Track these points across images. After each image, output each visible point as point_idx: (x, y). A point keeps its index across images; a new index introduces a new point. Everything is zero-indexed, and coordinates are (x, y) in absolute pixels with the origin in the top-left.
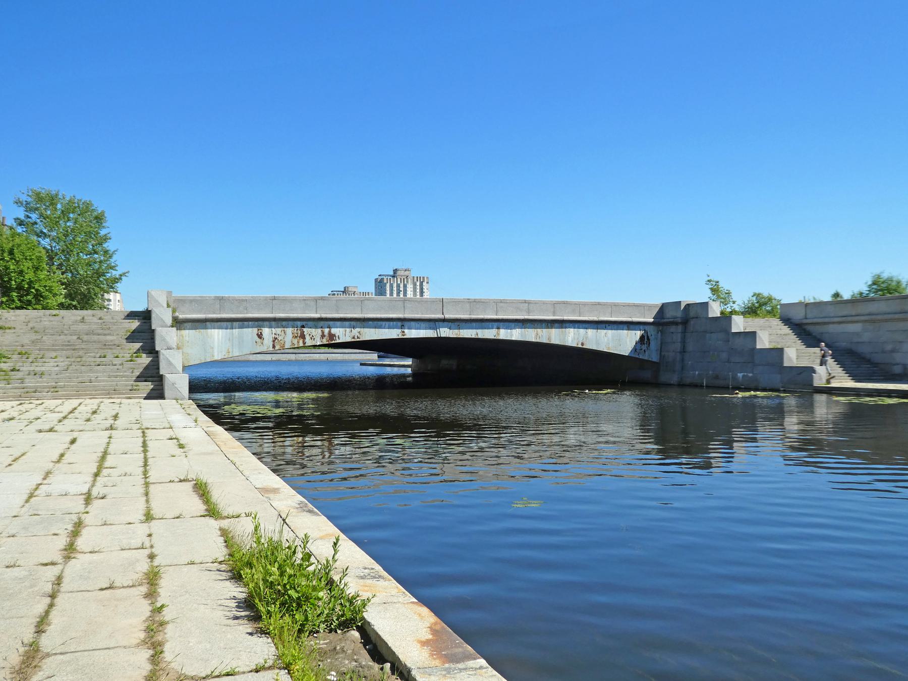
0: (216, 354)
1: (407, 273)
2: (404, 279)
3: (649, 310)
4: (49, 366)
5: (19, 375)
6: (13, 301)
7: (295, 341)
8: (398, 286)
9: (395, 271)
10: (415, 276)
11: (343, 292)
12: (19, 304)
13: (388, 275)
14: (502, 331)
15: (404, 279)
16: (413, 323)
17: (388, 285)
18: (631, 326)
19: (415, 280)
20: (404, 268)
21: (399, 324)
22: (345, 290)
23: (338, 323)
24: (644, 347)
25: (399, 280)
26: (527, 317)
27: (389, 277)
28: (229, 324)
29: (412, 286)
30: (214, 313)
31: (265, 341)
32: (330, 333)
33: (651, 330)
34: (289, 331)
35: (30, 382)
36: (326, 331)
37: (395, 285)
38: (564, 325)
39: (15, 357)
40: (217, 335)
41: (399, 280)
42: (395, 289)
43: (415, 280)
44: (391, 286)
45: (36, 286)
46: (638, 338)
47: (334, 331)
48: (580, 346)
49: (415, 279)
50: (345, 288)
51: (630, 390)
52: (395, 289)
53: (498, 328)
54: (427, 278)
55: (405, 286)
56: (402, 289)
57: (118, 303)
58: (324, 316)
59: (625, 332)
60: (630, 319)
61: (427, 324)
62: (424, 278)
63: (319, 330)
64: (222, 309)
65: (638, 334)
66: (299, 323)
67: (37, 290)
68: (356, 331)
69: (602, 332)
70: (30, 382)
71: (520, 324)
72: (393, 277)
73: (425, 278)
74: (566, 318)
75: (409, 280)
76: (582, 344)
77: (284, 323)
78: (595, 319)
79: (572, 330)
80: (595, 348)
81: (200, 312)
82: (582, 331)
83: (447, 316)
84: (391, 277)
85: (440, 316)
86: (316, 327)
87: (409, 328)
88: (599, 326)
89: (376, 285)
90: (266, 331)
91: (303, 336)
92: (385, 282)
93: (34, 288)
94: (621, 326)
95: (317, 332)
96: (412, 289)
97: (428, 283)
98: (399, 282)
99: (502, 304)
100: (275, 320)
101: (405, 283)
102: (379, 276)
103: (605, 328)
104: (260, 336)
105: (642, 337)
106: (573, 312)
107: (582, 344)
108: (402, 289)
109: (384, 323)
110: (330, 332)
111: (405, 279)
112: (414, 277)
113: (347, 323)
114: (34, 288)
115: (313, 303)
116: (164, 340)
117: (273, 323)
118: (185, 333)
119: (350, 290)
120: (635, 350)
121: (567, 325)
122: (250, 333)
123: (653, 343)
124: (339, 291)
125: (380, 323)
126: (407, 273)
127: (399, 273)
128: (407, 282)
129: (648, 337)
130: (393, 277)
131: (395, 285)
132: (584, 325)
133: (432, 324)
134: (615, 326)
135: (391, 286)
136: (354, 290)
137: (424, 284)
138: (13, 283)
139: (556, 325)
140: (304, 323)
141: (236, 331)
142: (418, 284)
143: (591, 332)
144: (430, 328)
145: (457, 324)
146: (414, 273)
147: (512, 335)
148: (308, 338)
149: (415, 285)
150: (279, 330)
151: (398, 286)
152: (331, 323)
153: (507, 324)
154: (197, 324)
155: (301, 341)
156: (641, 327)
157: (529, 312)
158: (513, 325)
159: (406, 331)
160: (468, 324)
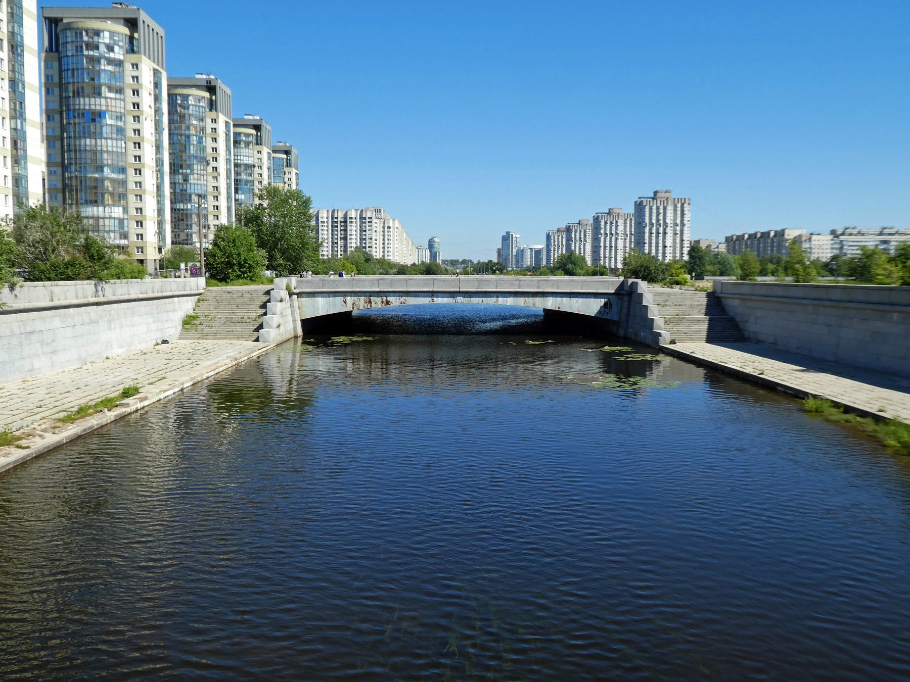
0: (320, 312)
1: (667, 195)
2: (664, 201)
3: (612, 284)
4: (217, 323)
5: (202, 327)
6: (236, 271)
7: (366, 305)
8: (658, 208)
9: (656, 193)
10: (626, 213)
11: (608, 213)
12: (239, 273)
13: (648, 198)
14: (500, 299)
15: (664, 201)
16: (439, 294)
17: (647, 208)
18: (597, 296)
19: (676, 202)
20: (665, 189)
21: (430, 294)
22: (609, 211)
23: (392, 294)
24: (607, 310)
25: (659, 202)
26: (517, 290)
27: (649, 199)
28: (328, 294)
29: (672, 208)
30: (319, 288)
31: (348, 305)
32: (386, 300)
33: (613, 298)
34: (362, 299)
35: (206, 331)
36: (384, 299)
37: (654, 208)
38: (545, 295)
39: (203, 318)
40: (320, 300)
41: (659, 202)
42: (654, 211)
43: (676, 202)
44: (651, 208)
45: (249, 262)
46: (602, 304)
47: (389, 299)
48: (557, 309)
49: (626, 215)
50: (579, 221)
51: (593, 345)
52: (654, 211)
53: (497, 297)
54: (689, 199)
55: (665, 208)
56: (661, 211)
57: (396, 230)
58: (382, 290)
59: (593, 299)
60: (595, 291)
61: (449, 295)
62: (685, 199)
63: (380, 298)
64: (323, 286)
65: (602, 302)
66: (368, 294)
67: (249, 264)
68: (402, 299)
69: (574, 300)
70: (206, 331)
71: (513, 295)
72: (653, 199)
73: (687, 200)
74: (546, 290)
75: (669, 202)
76: (559, 308)
77: (359, 294)
78: (568, 291)
79: (551, 298)
80: (568, 310)
81: (311, 288)
82: (559, 299)
83: (462, 290)
84: (651, 200)
85: (457, 290)
86: (378, 297)
87: (437, 297)
88: (572, 296)
89: (635, 207)
90: (349, 299)
91: (370, 302)
92: (644, 204)
93: (247, 263)
94: (589, 296)
95: (379, 300)
96: (672, 211)
97: (689, 204)
98: (659, 205)
99: (500, 282)
100: (353, 292)
101: (665, 205)
102: (639, 198)
103: (577, 297)
104: (345, 302)
105: (606, 304)
106: (553, 286)
107: (559, 308)
108: (661, 211)
109: (420, 294)
110: (386, 299)
111: (665, 202)
112: (674, 199)
113: (397, 294)
114: (247, 263)
115: (376, 282)
116: (271, 310)
117: (353, 294)
118: (303, 299)
119: (614, 211)
120: (600, 312)
121: (548, 295)
122: (339, 300)
123: (614, 307)
124: (603, 213)
125: (418, 294)
126: (667, 195)
127: (659, 195)
128: (667, 204)
129: (610, 303)
130: (653, 199)
131: (654, 208)
132: (560, 295)
133: (452, 295)
134: (585, 296)
135: (651, 208)
136: (618, 211)
137: (685, 205)
138: (234, 261)
139: (540, 295)
140: (371, 294)
141: (331, 299)
142: (679, 205)
143: (565, 300)
144: (451, 297)
145: (469, 294)
146: (673, 195)
147: (507, 302)
148: (373, 303)
149: (675, 207)
150: (356, 298)
151: (658, 208)
152: (387, 294)
153: (504, 294)
154: (310, 295)
155: (369, 305)
156: (605, 296)
157: (519, 286)
158: (508, 295)
159: (435, 299)
160: (477, 295)
